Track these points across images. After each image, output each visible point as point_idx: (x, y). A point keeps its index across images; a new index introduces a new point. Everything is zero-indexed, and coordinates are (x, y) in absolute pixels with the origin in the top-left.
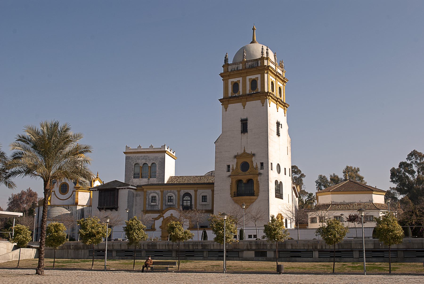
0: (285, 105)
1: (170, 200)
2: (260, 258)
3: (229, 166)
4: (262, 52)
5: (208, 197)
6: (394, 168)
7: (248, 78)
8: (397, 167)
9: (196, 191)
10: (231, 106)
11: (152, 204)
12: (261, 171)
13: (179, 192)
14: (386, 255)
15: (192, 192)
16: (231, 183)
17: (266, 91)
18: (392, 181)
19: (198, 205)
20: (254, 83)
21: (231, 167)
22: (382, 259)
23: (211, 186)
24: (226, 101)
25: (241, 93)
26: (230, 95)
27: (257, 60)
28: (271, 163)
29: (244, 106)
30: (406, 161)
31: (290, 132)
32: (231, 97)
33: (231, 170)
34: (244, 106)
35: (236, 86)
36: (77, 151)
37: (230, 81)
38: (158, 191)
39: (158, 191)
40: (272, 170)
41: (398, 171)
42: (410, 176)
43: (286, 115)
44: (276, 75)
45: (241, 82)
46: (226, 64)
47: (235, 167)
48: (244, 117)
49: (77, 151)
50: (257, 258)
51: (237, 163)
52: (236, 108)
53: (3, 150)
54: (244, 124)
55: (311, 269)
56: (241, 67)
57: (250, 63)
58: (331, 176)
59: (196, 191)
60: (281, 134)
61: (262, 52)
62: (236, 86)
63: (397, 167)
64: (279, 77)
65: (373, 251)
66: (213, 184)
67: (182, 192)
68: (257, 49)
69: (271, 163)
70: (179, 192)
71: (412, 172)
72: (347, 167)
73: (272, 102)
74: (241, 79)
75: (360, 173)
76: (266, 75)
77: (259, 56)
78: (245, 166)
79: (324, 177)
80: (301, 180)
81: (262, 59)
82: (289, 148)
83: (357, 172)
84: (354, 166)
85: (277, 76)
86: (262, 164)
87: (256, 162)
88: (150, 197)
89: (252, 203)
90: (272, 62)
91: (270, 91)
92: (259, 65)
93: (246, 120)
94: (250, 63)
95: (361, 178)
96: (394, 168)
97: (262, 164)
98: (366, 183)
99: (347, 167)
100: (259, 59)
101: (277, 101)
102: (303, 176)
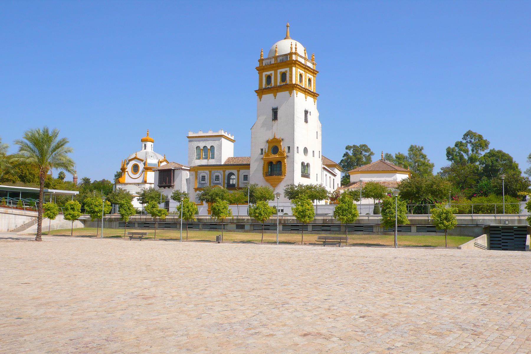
0: (314, 95)
1: (217, 178)
2: (240, 230)
3: (262, 150)
4: (291, 48)
5: (206, 177)
6: (449, 148)
7: (279, 71)
8: (452, 146)
9: (238, 171)
10: (265, 97)
11: (203, 182)
12: (288, 154)
13: (224, 172)
14: (332, 229)
15: (235, 172)
16: (264, 165)
17: (294, 82)
18: (448, 159)
19: (240, 183)
20: (284, 76)
21: (264, 150)
22: (329, 232)
23: (248, 166)
24: (261, 92)
25: (273, 85)
26: (264, 87)
27: (286, 55)
28: (298, 147)
29: (275, 97)
30: (462, 140)
31: (321, 118)
32: (265, 89)
33: (264, 153)
34: (275, 97)
35: (269, 78)
36: (60, 145)
37: (264, 74)
38: (207, 172)
39: (207, 172)
40: (298, 152)
41: (453, 150)
42: (464, 154)
43: (316, 103)
44: (305, 68)
45: (273, 75)
46: (261, 61)
47: (267, 150)
48: (275, 106)
49: (60, 145)
50: (237, 230)
51: (269, 147)
52: (268, 97)
53: (5, 143)
54: (275, 112)
55: (340, 238)
56: (273, 61)
57: (281, 58)
58: (396, 155)
59: (238, 171)
60: (308, 121)
61: (291, 48)
62: (269, 78)
63: (452, 146)
64: (308, 70)
65: (323, 226)
66: (249, 165)
67: (227, 172)
68: (285, 46)
69: (298, 147)
70: (224, 172)
71: (466, 152)
72: (412, 146)
73: (299, 93)
74: (273, 72)
75: (424, 152)
76: (294, 69)
77: (288, 51)
78: (275, 150)
79: (390, 155)
80: (370, 158)
81: (291, 54)
82: (320, 133)
83: (421, 150)
84: (419, 144)
85: (306, 68)
86: (289, 148)
87: (284, 146)
88: (201, 177)
89: (280, 182)
90: (301, 57)
91: (298, 83)
92: (288, 59)
93: (277, 109)
94: (281, 58)
95: (424, 157)
96: (449, 148)
97: (289, 148)
98: (428, 161)
99: (412, 146)
100: (289, 54)
101: (306, 91)
102: (372, 154)
